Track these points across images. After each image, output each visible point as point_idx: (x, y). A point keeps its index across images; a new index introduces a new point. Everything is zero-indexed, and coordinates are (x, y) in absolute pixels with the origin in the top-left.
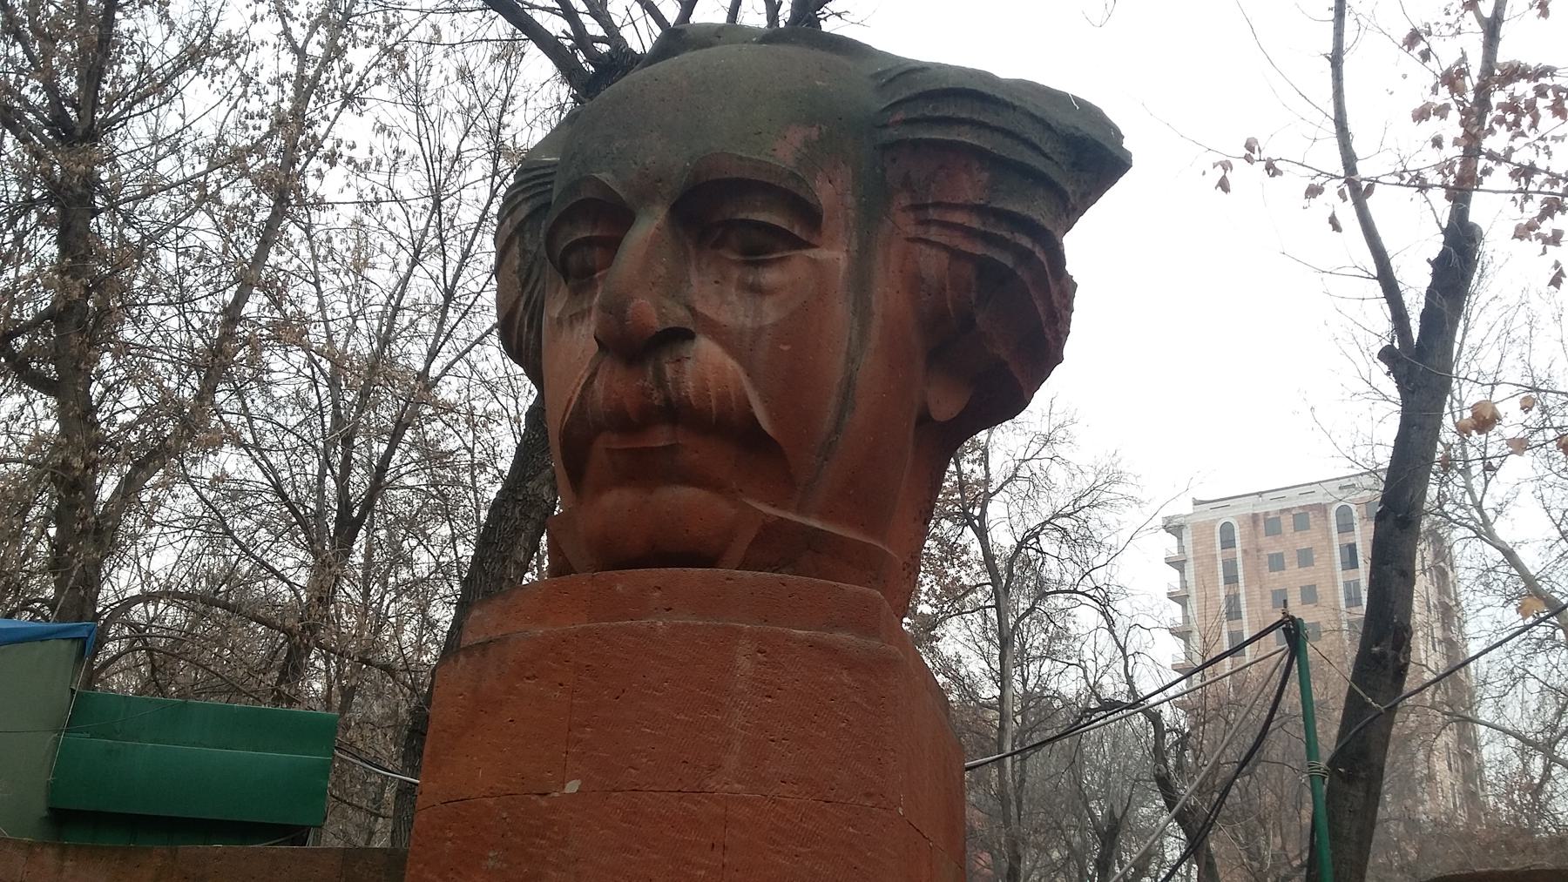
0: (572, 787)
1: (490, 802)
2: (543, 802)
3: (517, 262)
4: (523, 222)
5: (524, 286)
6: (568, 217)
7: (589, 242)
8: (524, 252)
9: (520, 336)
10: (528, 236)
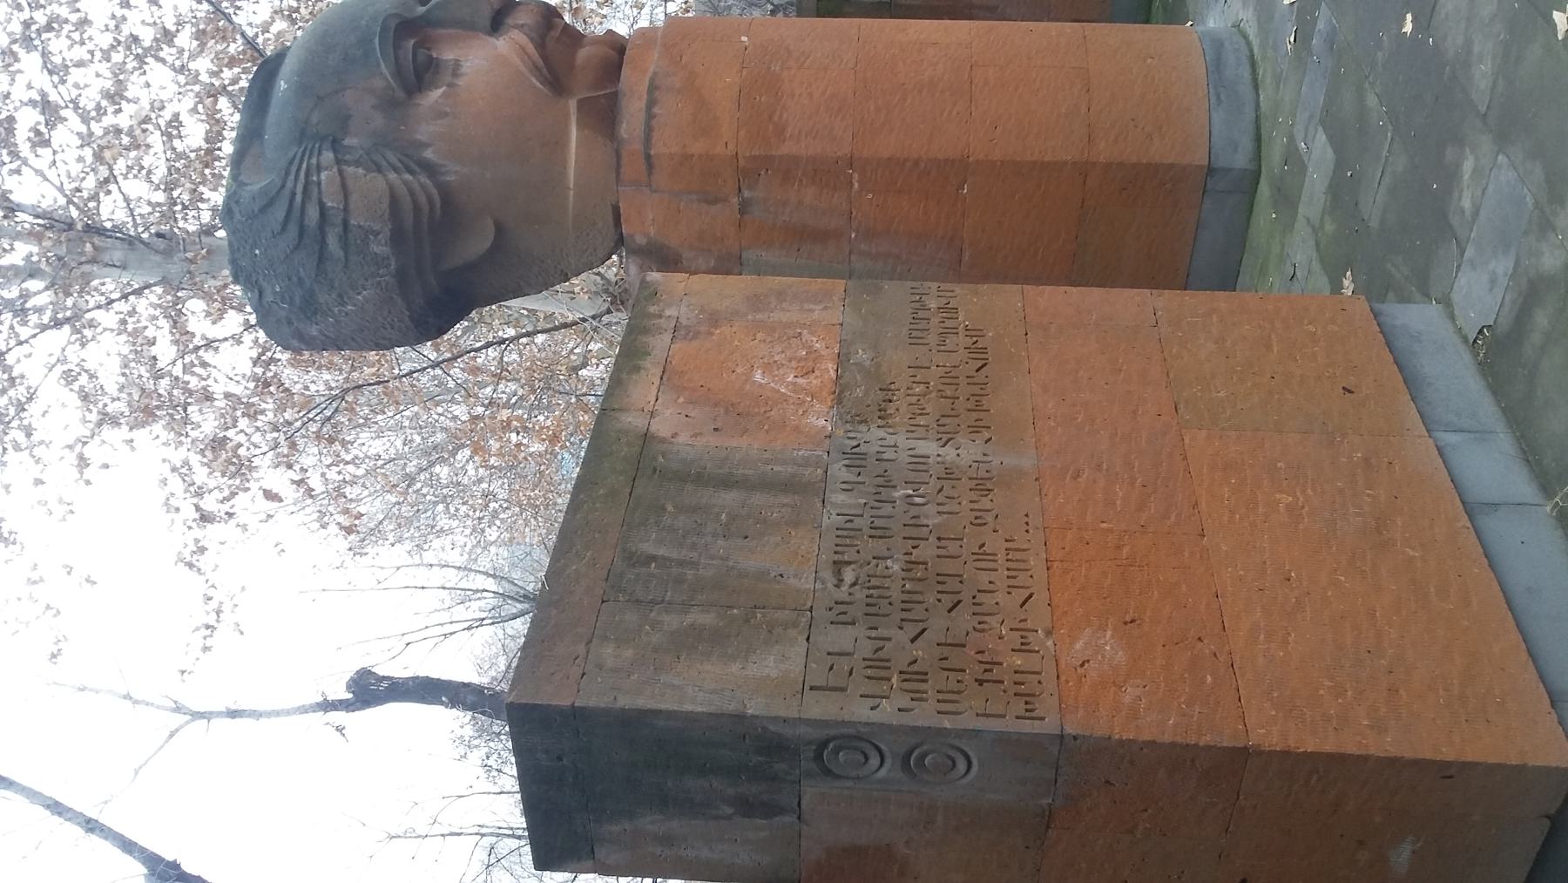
0: (744, 39)
5: (379, 170)
6: (396, 47)
8: (357, 163)
9: (412, 193)
10: (348, 157)
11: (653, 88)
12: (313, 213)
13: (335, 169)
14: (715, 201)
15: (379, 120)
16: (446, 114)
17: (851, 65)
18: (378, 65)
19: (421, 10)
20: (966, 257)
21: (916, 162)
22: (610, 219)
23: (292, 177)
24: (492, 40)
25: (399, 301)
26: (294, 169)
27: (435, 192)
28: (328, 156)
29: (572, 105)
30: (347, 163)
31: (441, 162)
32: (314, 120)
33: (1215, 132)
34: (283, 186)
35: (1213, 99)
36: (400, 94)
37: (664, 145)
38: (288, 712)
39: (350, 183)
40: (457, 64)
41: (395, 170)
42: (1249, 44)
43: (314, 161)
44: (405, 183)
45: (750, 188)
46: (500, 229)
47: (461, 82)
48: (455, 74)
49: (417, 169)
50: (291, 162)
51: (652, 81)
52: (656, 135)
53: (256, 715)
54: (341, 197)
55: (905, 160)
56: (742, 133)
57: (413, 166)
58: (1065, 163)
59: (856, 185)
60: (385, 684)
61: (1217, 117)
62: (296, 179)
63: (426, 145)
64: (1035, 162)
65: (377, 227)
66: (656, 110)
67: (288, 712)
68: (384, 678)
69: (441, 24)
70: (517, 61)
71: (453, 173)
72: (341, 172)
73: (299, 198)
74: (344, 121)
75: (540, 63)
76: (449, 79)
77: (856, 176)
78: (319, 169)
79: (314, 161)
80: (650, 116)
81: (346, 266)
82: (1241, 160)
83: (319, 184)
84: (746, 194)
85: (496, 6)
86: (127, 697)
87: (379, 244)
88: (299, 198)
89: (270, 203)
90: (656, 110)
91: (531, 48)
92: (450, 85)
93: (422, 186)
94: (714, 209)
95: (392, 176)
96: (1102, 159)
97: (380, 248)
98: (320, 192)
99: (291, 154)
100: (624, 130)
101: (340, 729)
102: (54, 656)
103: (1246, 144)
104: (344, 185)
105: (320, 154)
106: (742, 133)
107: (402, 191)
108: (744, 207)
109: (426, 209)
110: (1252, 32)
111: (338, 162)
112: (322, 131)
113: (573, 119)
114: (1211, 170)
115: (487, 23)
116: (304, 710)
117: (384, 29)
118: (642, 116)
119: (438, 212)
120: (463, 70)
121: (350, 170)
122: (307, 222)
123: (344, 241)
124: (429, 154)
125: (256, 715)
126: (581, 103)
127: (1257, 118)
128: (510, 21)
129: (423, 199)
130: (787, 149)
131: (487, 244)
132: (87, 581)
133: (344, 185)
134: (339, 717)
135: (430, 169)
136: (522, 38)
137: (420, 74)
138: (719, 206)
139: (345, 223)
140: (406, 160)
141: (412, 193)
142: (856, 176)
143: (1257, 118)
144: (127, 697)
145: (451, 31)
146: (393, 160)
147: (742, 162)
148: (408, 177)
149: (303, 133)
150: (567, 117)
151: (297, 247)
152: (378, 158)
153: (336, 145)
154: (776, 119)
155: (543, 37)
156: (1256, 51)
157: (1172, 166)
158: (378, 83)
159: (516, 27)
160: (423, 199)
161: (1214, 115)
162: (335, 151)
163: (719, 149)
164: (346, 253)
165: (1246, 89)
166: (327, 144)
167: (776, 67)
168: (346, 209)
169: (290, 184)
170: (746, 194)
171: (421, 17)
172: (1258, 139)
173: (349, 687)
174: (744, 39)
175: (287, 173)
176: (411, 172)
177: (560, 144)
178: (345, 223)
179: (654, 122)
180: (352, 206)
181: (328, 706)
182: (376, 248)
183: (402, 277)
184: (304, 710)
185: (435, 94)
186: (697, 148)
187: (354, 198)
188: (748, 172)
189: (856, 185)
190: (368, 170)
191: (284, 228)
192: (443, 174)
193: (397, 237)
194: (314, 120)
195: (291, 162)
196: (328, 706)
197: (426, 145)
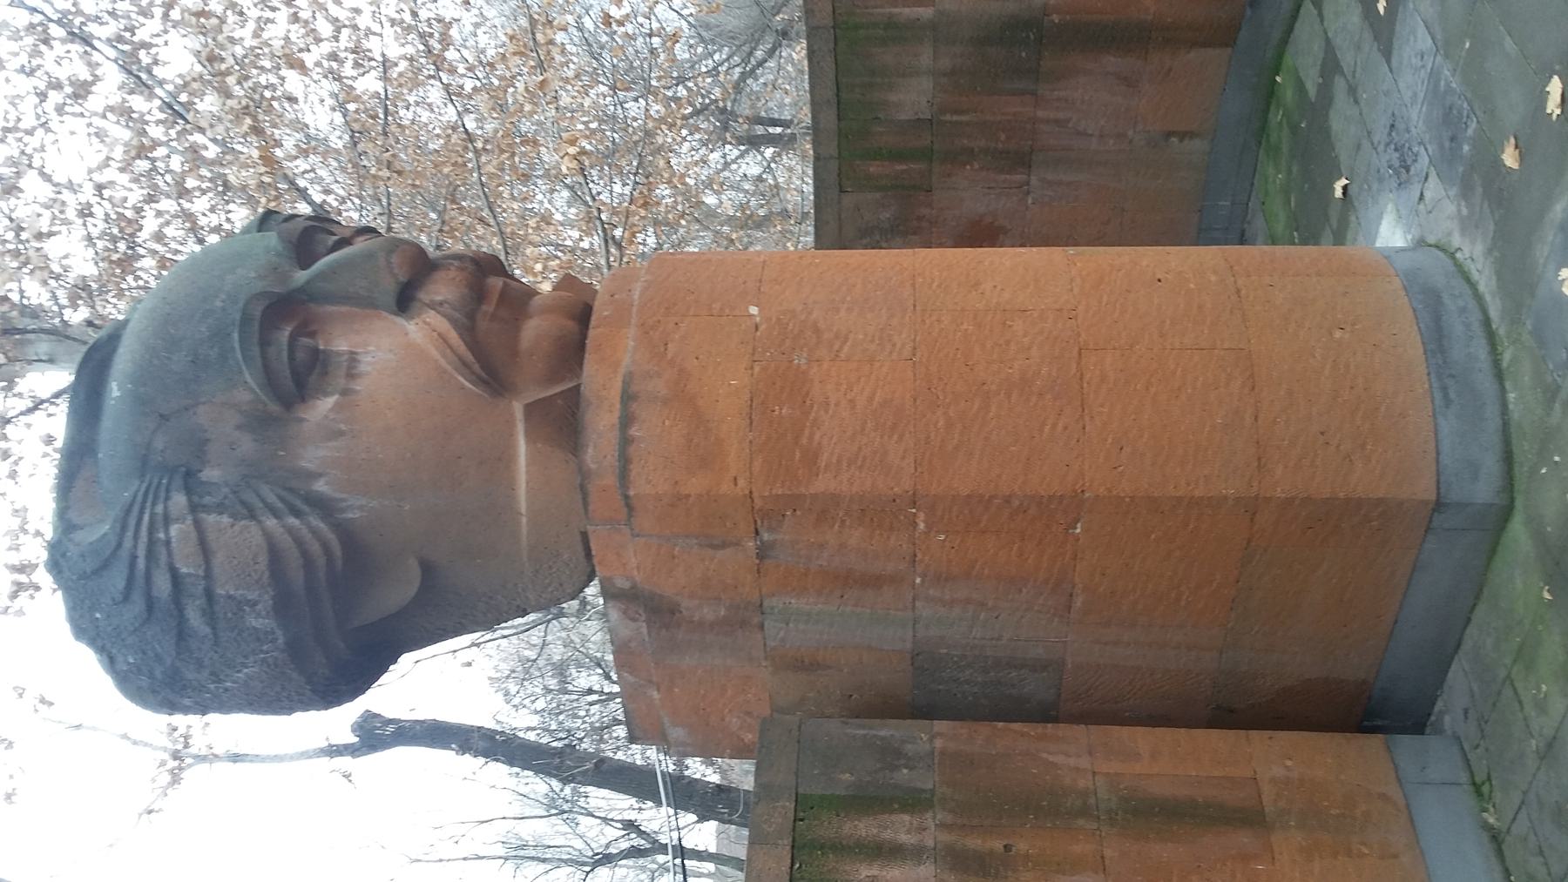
0: (754, 310)
1: (757, 369)
2: (762, 327)
3: (225, 519)
4: (190, 500)
5: (252, 515)
6: (264, 343)
7: (293, 338)
8: (220, 508)
9: (299, 542)
10: (207, 500)
11: (628, 397)
12: (162, 585)
13: (189, 520)
14: (723, 546)
15: (247, 445)
16: (341, 433)
17: (907, 353)
18: (241, 372)
19: (301, 276)
20: (1078, 602)
21: (1007, 500)
22: (580, 548)
23: (130, 534)
24: (400, 320)
25: (295, 675)
26: (132, 522)
27: (331, 537)
28: (179, 500)
29: (518, 408)
30: (207, 509)
31: (338, 495)
32: (159, 444)
33: (1446, 446)
34: (119, 545)
35: (1438, 395)
36: (274, 408)
37: (649, 481)
38: (292, 758)
39: (211, 536)
40: (353, 358)
41: (276, 514)
42: (1478, 297)
43: (159, 509)
44: (290, 531)
45: (771, 529)
46: (427, 568)
47: (358, 386)
48: (351, 375)
49: (305, 508)
50: (128, 511)
51: (627, 384)
52: (635, 469)
53: (256, 758)
54: (200, 560)
55: (992, 497)
56: (757, 464)
57: (298, 503)
58: (1226, 498)
59: (922, 526)
60: (391, 728)
61: (1447, 426)
62: (141, 512)
63: (313, 476)
64: (1179, 499)
65: (252, 596)
66: (634, 431)
67: (292, 758)
68: (391, 721)
69: (329, 298)
70: (435, 353)
71: (356, 509)
72: (198, 524)
73: (141, 563)
74: (199, 446)
75: (469, 357)
76: (342, 382)
77: (922, 516)
78: (167, 520)
79: (159, 509)
80: (626, 441)
81: (216, 643)
82: (1484, 491)
83: (168, 543)
84: (766, 536)
85: (403, 279)
86: (125, 737)
87: (259, 615)
88: (141, 563)
89: (105, 565)
90: (634, 431)
91: (454, 337)
92: (345, 392)
93: (314, 532)
94: (720, 554)
95: (271, 523)
96: (1279, 493)
97: (259, 621)
98: (170, 554)
99: (134, 488)
100: (590, 455)
101: (347, 776)
102: (9, 797)
103: (1491, 464)
104: (203, 543)
105: (167, 498)
106: (757, 464)
107: (286, 541)
108: (763, 552)
109: (321, 561)
110: (1486, 282)
111: (194, 508)
112: (173, 467)
113: (520, 428)
114: (1439, 505)
115: (391, 299)
116: (306, 755)
117: (246, 320)
118: (613, 437)
119: (339, 564)
120: (363, 368)
121: (210, 519)
122: (155, 593)
123: (210, 615)
124: (320, 486)
125: (256, 758)
126: (530, 409)
127: (1506, 425)
128: (422, 296)
129: (315, 548)
130: (822, 484)
131: (417, 584)
132: (43, 701)
133: (203, 543)
134: (345, 762)
135: (323, 506)
136: (443, 325)
137: (300, 376)
138: (728, 551)
139: (209, 594)
140: (284, 493)
141: (299, 542)
142: (922, 516)
143: (1506, 425)
144: (125, 737)
145: (344, 309)
146: (272, 498)
147: (758, 503)
148: (293, 521)
149: (144, 461)
150: (510, 423)
151: (148, 620)
152: (249, 497)
153: (190, 481)
154: (804, 441)
155: (471, 316)
156: (1494, 313)
157: (1380, 501)
158: (243, 396)
159: (433, 306)
160: (315, 548)
161: (1441, 420)
162: (189, 491)
163: (726, 488)
164: (214, 628)
165: (1485, 382)
166: (178, 481)
167: (800, 360)
168: (208, 575)
169: (128, 543)
170: (766, 536)
171: (301, 290)
172: (1508, 458)
173: (353, 731)
174: (754, 310)
175: (124, 528)
176: (297, 513)
177: (505, 458)
178: (209, 594)
179: (632, 449)
180: (217, 571)
181: (334, 751)
182: (253, 622)
183: (295, 650)
184: (306, 755)
185: (325, 405)
186: (695, 485)
187: (219, 559)
188: (765, 516)
189: (922, 526)
190: (233, 516)
191: (126, 597)
192: (343, 510)
193: (283, 606)
194: (159, 444)
195: (128, 511)
196: (334, 751)
197: (313, 476)
